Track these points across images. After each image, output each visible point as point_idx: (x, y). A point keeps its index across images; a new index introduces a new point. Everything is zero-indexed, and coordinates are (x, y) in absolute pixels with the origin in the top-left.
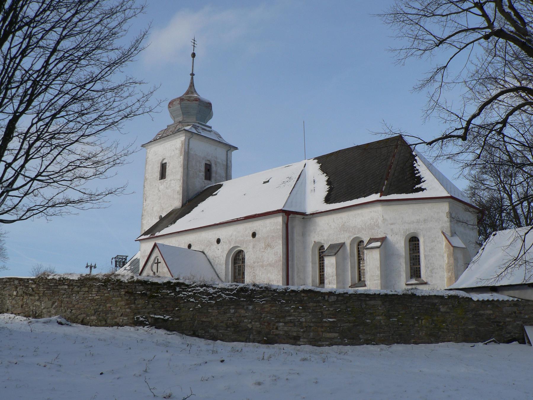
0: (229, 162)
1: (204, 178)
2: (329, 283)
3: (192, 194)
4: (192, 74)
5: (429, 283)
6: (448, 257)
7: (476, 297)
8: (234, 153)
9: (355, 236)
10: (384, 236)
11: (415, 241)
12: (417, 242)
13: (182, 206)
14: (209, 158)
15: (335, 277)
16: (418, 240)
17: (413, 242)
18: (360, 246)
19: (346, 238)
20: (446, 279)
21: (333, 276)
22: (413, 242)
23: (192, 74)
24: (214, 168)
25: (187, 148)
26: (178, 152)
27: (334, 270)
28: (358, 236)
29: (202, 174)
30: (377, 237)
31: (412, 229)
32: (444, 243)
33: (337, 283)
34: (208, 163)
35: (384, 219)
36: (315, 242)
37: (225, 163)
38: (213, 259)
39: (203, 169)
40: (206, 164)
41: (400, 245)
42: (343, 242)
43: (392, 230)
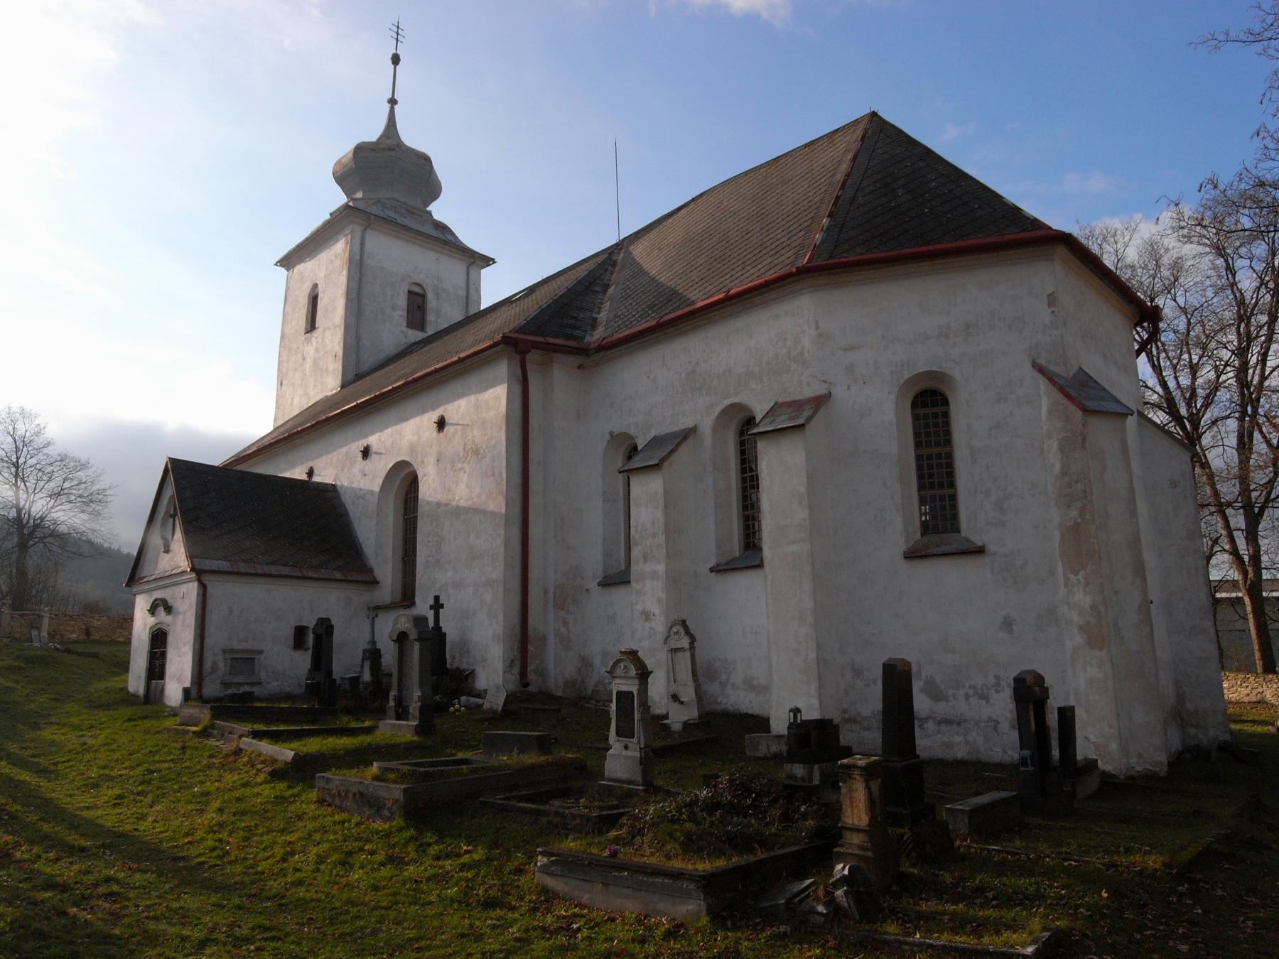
0: (472, 292)
1: (404, 324)
2: (645, 557)
3: (369, 360)
4: (393, 102)
5: (991, 547)
6: (1062, 450)
7: (286, 571)
8: (485, 272)
9: (728, 402)
10: (820, 390)
11: (934, 404)
12: (939, 410)
13: (343, 387)
14: (420, 278)
15: (662, 538)
16: (946, 402)
17: (929, 405)
18: (746, 432)
19: (699, 412)
20: (1057, 534)
21: (654, 535)
22: (929, 405)
23: (393, 102)
24: (432, 302)
25: (357, 250)
26: (338, 263)
27: (659, 514)
28: (736, 400)
29: (400, 315)
30: (798, 397)
31: (923, 359)
32: (1045, 404)
33: (668, 556)
34: (416, 289)
35: (820, 336)
36: (611, 433)
37: (462, 293)
38: (353, 503)
39: (402, 302)
40: (410, 292)
41: (881, 418)
42: (690, 424)
43: (850, 368)
